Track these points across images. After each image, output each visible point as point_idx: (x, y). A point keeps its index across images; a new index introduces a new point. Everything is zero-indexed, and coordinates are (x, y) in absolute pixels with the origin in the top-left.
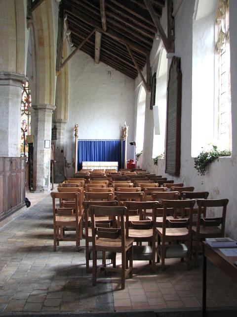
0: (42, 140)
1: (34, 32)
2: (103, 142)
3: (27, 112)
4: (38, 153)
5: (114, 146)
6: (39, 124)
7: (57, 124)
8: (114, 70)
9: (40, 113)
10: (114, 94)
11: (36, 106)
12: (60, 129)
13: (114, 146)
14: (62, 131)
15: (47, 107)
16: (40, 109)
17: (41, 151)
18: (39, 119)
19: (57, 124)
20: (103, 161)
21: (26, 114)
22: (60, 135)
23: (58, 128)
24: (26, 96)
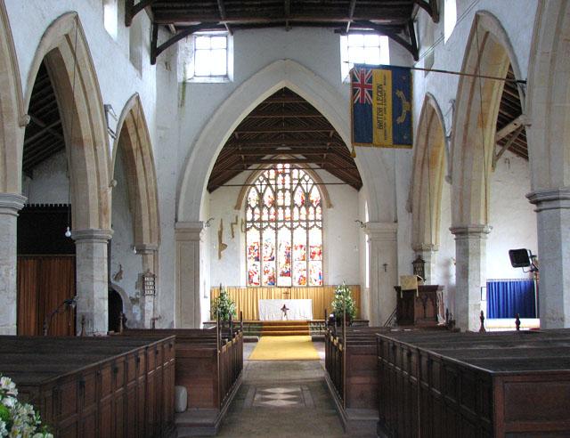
0: (477, 286)
1: (470, 103)
2: (505, 284)
3: (273, 224)
4: (470, 309)
5: (523, 288)
6: (470, 258)
7: (424, 254)
8: (515, 156)
9: (471, 241)
10: (517, 198)
11: (467, 228)
12: (430, 263)
13: (523, 288)
14: (432, 265)
15: (470, 230)
16: (471, 232)
17: (475, 305)
18: (470, 251)
19: (424, 254)
20: (504, 317)
21: (271, 227)
22: (429, 273)
23: (425, 259)
24: (272, 195)
